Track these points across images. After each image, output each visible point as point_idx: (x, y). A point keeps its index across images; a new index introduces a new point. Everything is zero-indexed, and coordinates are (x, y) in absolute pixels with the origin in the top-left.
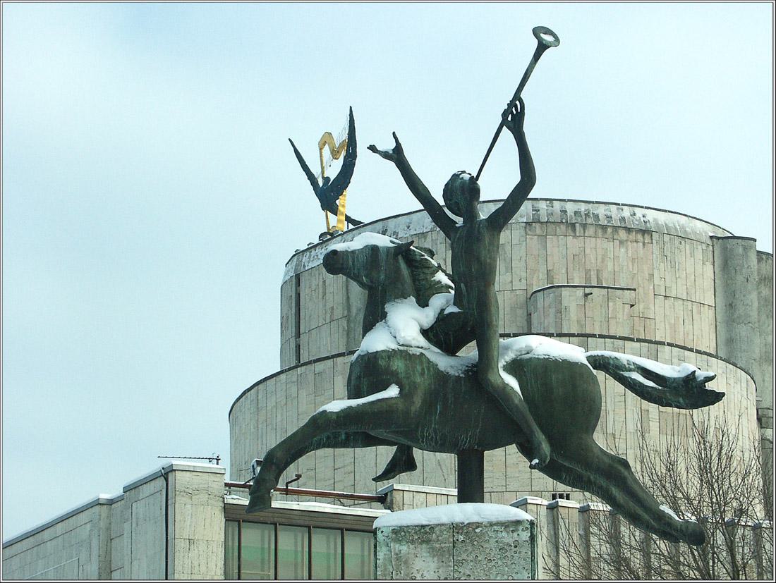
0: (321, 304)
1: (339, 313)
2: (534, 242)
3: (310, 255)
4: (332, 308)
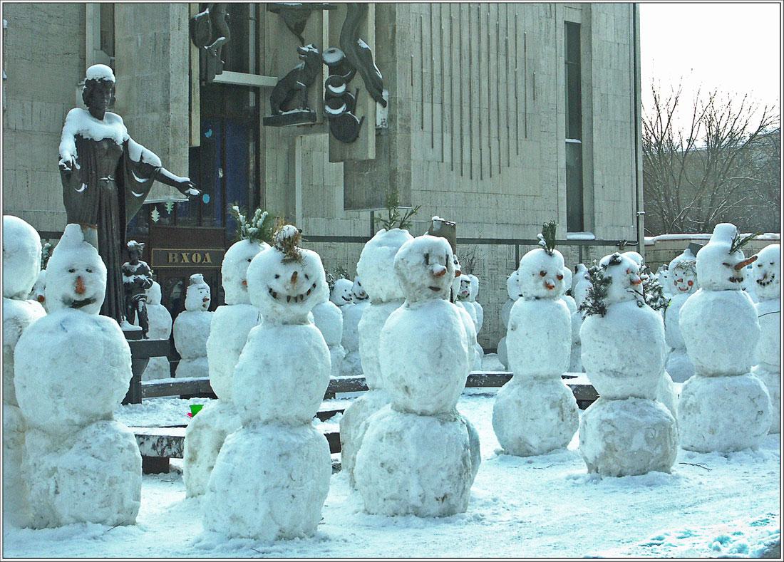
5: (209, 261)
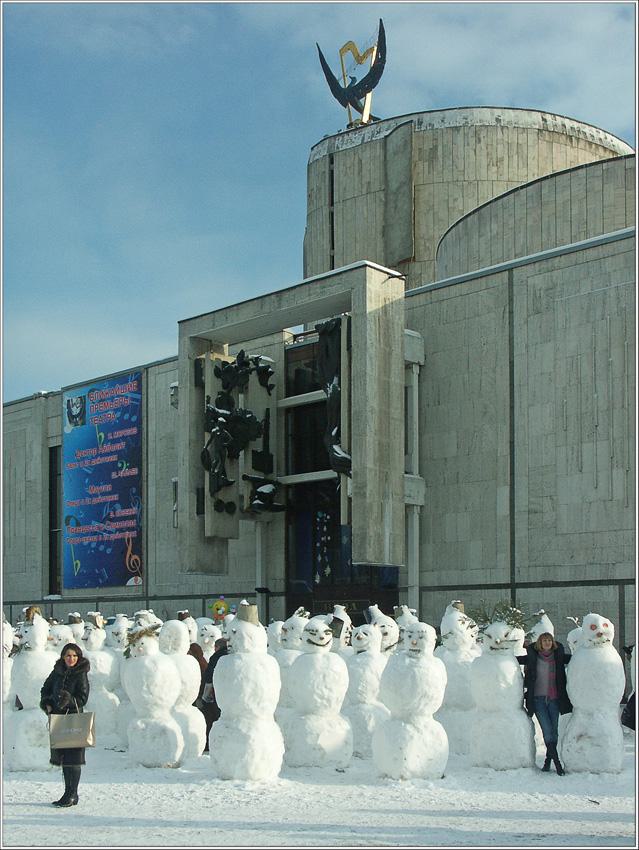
0: (357, 179)
1: (376, 186)
2: (544, 146)
3: (343, 141)
4: (369, 183)
5: (355, 608)
